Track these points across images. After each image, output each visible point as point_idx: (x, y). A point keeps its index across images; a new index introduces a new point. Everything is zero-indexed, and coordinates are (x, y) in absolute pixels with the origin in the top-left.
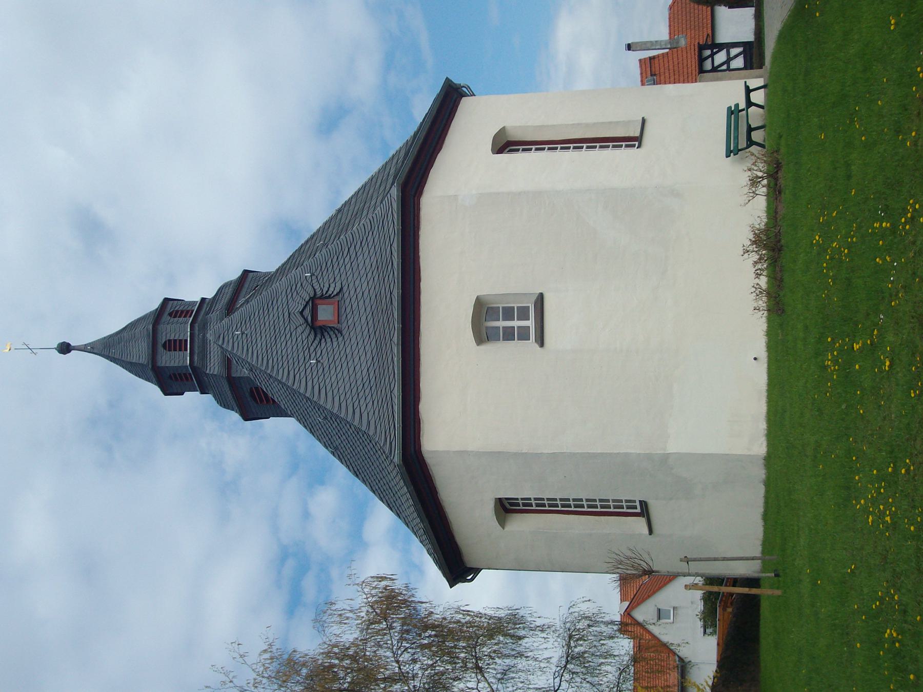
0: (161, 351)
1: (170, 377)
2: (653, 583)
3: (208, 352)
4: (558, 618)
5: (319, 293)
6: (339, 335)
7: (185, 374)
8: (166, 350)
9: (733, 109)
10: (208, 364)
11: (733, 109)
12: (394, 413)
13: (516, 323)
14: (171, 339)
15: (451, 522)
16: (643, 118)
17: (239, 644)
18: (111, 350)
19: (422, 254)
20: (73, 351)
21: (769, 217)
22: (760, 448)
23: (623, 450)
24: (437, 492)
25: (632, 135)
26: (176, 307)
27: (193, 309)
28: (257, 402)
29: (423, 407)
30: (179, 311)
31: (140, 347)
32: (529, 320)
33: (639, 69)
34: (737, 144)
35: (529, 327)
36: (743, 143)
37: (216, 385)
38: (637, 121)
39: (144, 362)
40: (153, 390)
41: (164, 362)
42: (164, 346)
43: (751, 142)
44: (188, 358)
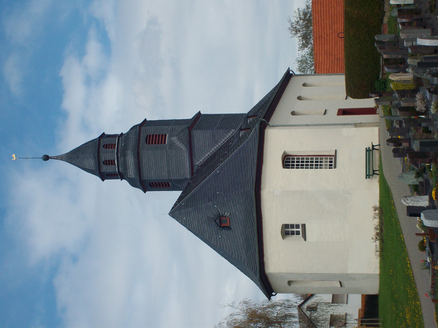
0: (102, 165)
1: (107, 175)
2: (331, 26)
5: (221, 215)
8: (105, 164)
9: (368, 149)
10: (129, 173)
11: (368, 149)
13: (295, 230)
14: (109, 159)
15: (267, 275)
18: (73, 160)
19: (262, 210)
20: (50, 159)
21: (381, 223)
22: (378, 272)
23: (333, 272)
25: (331, 154)
26: (105, 142)
27: (115, 143)
29: (265, 259)
34: (369, 172)
35: (300, 231)
37: (133, 184)
39: (92, 168)
40: (98, 179)
42: (104, 163)
43: (374, 174)
44: (117, 169)
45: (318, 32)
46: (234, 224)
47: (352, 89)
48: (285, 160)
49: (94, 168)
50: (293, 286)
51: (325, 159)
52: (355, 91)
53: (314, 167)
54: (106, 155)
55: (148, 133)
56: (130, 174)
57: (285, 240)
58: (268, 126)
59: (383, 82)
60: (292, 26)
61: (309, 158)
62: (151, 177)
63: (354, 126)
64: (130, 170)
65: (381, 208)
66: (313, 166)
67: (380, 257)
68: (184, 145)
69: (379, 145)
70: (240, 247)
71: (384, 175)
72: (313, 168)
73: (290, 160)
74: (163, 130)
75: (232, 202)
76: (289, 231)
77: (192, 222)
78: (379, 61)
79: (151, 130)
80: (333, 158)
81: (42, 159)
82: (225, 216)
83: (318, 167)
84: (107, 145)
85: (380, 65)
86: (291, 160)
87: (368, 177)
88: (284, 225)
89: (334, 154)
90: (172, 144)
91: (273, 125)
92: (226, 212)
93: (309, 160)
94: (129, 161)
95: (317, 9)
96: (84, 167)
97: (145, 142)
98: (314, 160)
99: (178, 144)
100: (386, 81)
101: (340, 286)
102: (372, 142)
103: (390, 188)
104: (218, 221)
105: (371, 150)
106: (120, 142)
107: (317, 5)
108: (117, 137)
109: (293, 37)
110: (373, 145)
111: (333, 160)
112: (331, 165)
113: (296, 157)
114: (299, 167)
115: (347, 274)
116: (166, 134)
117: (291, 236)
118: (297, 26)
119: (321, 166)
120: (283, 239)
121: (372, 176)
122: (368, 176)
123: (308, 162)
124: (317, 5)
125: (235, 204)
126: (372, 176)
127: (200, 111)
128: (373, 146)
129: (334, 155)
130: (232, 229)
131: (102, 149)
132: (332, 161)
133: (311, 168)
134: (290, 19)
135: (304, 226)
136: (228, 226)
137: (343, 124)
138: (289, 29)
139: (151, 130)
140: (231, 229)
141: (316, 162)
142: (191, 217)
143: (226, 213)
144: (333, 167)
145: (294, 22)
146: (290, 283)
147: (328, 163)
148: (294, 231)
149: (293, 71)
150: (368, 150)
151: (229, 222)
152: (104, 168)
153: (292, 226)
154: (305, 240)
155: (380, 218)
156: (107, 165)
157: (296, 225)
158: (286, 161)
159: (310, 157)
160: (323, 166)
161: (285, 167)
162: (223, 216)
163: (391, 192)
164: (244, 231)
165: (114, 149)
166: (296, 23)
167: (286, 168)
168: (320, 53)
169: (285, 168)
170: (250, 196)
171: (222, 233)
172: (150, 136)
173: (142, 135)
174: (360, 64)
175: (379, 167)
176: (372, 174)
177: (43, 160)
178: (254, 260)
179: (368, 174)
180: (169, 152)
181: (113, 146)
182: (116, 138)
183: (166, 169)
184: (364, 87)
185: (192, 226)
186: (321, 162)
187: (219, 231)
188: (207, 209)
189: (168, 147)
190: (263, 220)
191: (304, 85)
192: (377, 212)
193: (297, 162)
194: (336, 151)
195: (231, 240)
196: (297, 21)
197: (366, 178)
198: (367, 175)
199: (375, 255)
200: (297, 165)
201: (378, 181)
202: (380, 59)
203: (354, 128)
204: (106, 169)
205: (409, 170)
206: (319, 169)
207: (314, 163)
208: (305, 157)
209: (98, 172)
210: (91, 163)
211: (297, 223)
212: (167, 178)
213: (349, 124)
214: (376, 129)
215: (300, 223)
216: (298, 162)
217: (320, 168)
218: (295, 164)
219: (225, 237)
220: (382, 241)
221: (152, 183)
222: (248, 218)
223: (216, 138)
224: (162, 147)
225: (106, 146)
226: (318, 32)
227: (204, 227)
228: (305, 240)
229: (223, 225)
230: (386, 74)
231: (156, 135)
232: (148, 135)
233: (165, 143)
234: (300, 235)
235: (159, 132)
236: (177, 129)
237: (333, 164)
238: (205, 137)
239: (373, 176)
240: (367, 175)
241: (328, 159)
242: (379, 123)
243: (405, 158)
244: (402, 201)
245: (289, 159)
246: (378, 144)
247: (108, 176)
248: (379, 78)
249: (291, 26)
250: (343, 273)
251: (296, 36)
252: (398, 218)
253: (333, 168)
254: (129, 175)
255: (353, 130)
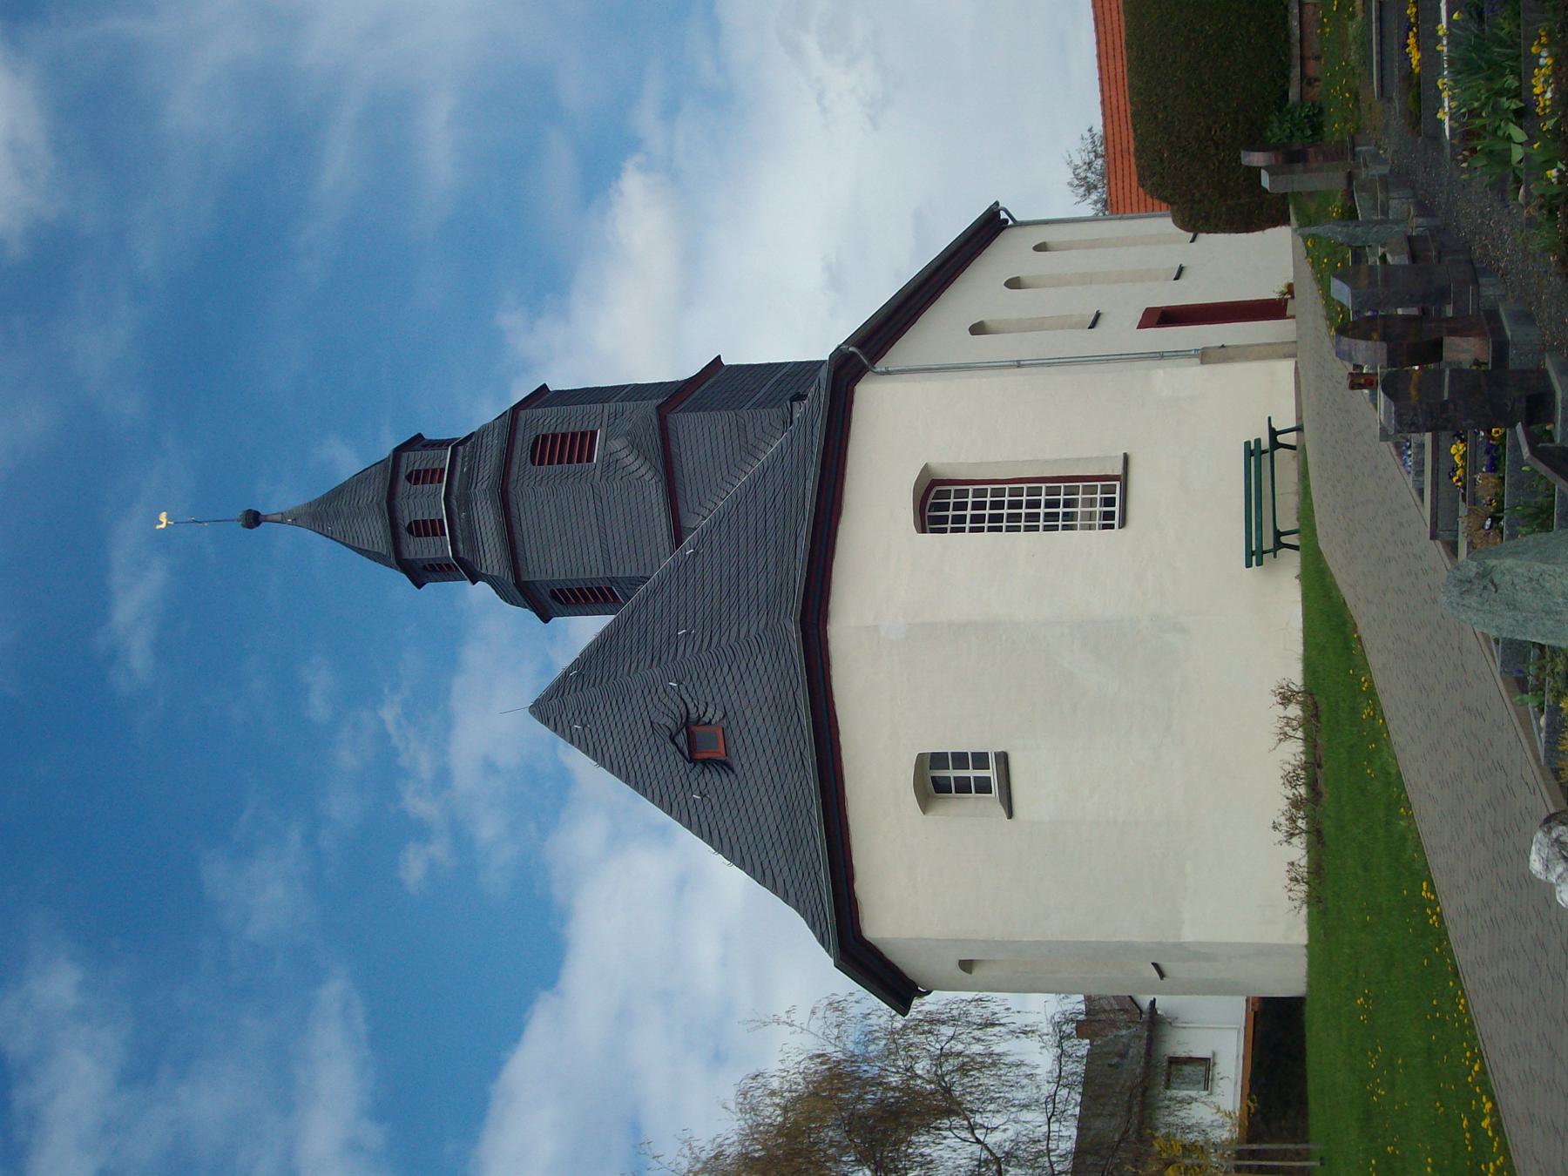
3: (480, 544)
4: (1045, 1022)
6: (730, 772)
7: (446, 565)
8: (413, 535)
9: (1252, 447)
10: (483, 561)
11: (1252, 447)
12: (822, 892)
13: (971, 773)
16: (1125, 454)
17: (649, 1143)
20: (263, 524)
21: (1311, 870)
24: (882, 954)
25: (1110, 473)
27: (442, 466)
28: (562, 603)
30: (420, 470)
31: (372, 529)
32: (989, 769)
33: (1099, 94)
35: (990, 778)
36: (1268, 543)
38: (1116, 457)
41: (413, 553)
42: (409, 530)
43: (1278, 545)
44: (449, 547)
45: (1118, 141)
46: (742, 751)
47: (1162, 161)
48: (930, 501)
49: (383, 546)
50: (978, 973)
51: (1087, 490)
52: (1176, 168)
53: (1041, 523)
54: (428, 503)
55: (540, 429)
56: (489, 562)
57: (931, 817)
58: (870, 372)
59: (1306, 116)
60: (1076, 176)
61: (1023, 488)
62: (550, 571)
63: (1197, 360)
64: (487, 551)
65: (1311, 694)
66: (1039, 521)
67: (1309, 904)
68: (648, 464)
69: (1299, 429)
70: (767, 838)
71: (1321, 553)
72: (1036, 529)
73: (949, 498)
74: (586, 418)
75: (726, 669)
76: (950, 778)
77: (603, 742)
78: (1286, 17)
79: (549, 420)
80: (1115, 485)
81: (240, 523)
82: (707, 721)
83: (1058, 526)
84: (418, 472)
85: (1287, 39)
86: (952, 500)
87: (1254, 558)
88: (929, 757)
89: (1118, 471)
90: (610, 463)
91: (890, 369)
92: (709, 704)
93: (1060, 495)
94: (482, 523)
95: (1112, 74)
96: (356, 545)
97: (529, 458)
98: (1043, 498)
99: (630, 460)
100: (1321, 111)
101: (1155, 974)
102: (1270, 419)
103: (1354, 613)
104: (681, 739)
105: (1267, 452)
106: (459, 460)
107: (1111, 61)
108: (448, 446)
109: (1079, 202)
110: (1274, 429)
111: (1117, 496)
112: (1109, 516)
113: (971, 488)
114: (946, 529)
115: (1180, 946)
116: (595, 429)
117: (958, 798)
118: (1089, 175)
119: (1072, 521)
120: (924, 813)
121: (1272, 554)
122: (1254, 555)
123: (1018, 505)
124: (1111, 61)
125: (738, 678)
126: (1272, 554)
127: (719, 357)
128: (1273, 434)
129: (1120, 473)
130: (738, 769)
131: (403, 485)
132: (1114, 498)
133: (1028, 529)
134: (1070, 156)
135: (1003, 759)
136: (723, 759)
137: (1158, 355)
138: (1070, 184)
139: (549, 420)
140: (733, 772)
141: (1049, 504)
142: (598, 723)
143: (711, 710)
144: (1116, 522)
145: (1081, 164)
146: (967, 966)
147: (1098, 509)
148: (969, 777)
149: (1010, 211)
150: (1252, 452)
151: (722, 746)
152: (411, 547)
153: (960, 760)
154: (1010, 815)
155: (1311, 743)
156: (419, 535)
157: (972, 753)
158: (932, 504)
159: (1025, 486)
160: (1077, 520)
161: (928, 527)
162: (700, 723)
163: (1356, 632)
164: (776, 779)
165: (438, 485)
166: (1085, 167)
167: (933, 531)
168: (1128, 201)
169: (928, 530)
170: (787, 644)
171: (703, 785)
172: (545, 437)
173: (519, 436)
174: (1192, 35)
175: (1298, 519)
176: (1272, 547)
177: (244, 526)
178: (816, 892)
179: (1254, 549)
180: (601, 489)
181: (432, 475)
182: (447, 449)
183: (597, 542)
184: (1217, 149)
185: (603, 756)
186: (1067, 504)
187: (692, 777)
188: (646, 692)
189: (598, 472)
190: (844, 739)
191: (1041, 248)
192: (1294, 711)
193: (976, 506)
194: (1126, 458)
195: (735, 812)
196: (1088, 161)
197: (1249, 565)
198: (1253, 553)
199: (1289, 898)
200: (975, 519)
201: (1295, 575)
202: (1286, 8)
203: (1197, 365)
204: (419, 549)
205: (1488, 523)
206: (1060, 534)
207: (1042, 510)
208: (1007, 486)
209: (393, 560)
210: (374, 530)
211: (979, 748)
212: (601, 575)
213: (1179, 353)
214: (1286, 368)
215: (991, 748)
216: (981, 506)
217: (1065, 528)
218: (969, 512)
219: (714, 800)
220: (1317, 839)
221: (561, 591)
222: (785, 730)
223: (750, 437)
224: (579, 474)
225: (416, 477)
226: (1118, 141)
227: (641, 759)
228: (1010, 815)
229: (699, 756)
230: (1317, 80)
231: (564, 436)
232: (538, 436)
233: (590, 459)
234: (991, 793)
235: (572, 425)
236: (631, 414)
237: (1116, 509)
238: (713, 434)
239: (1275, 556)
240: (1249, 554)
241: (1096, 493)
242: (1295, 342)
243: (1453, 451)
244: (1536, 865)
245: (947, 494)
246: (1293, 425)
247: (436, 571)
248: (1287, 100)
249: (1073, 176)
250: (1164, 940)
251: (1089, 201)
252: (1399, 775)
253: (1116, 526)
254: (484, 566)
255: (1196, 373)
